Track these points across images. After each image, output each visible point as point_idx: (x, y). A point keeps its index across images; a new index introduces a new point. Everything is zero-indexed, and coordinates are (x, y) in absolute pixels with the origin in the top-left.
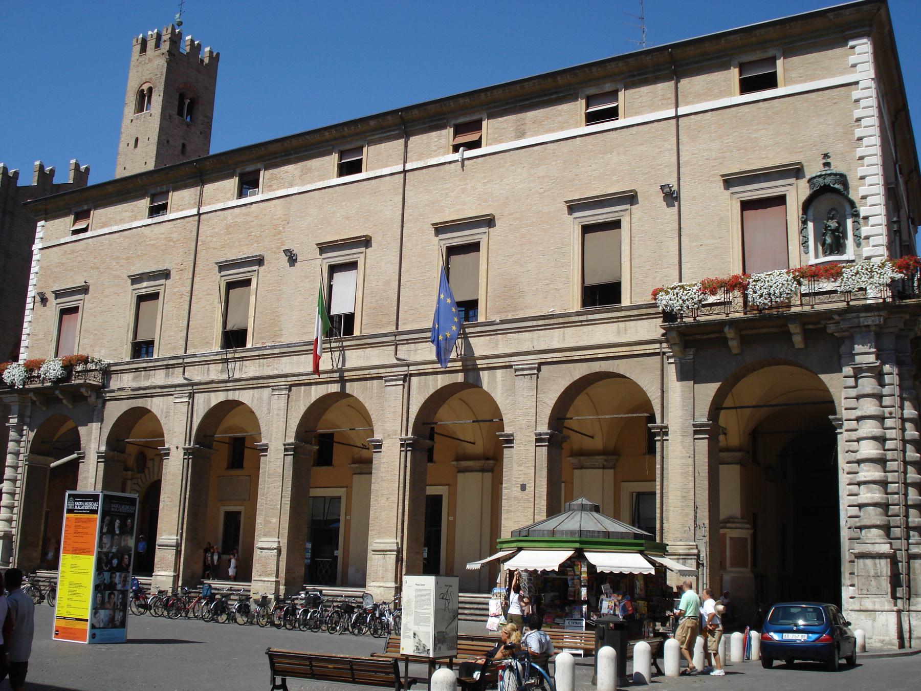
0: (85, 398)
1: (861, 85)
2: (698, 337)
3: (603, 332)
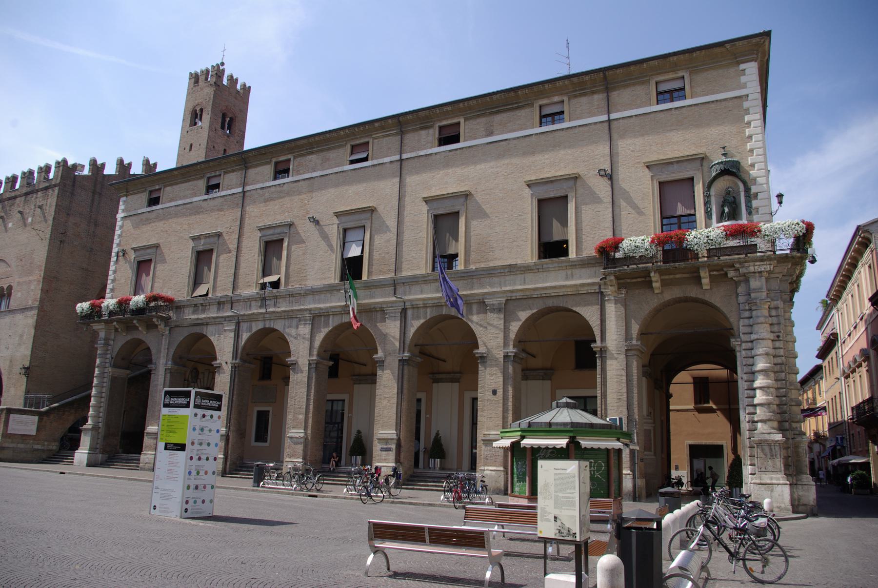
0: (156, 326)
1: (750, 97)
2: (629, 281)
3: (555, 280)
